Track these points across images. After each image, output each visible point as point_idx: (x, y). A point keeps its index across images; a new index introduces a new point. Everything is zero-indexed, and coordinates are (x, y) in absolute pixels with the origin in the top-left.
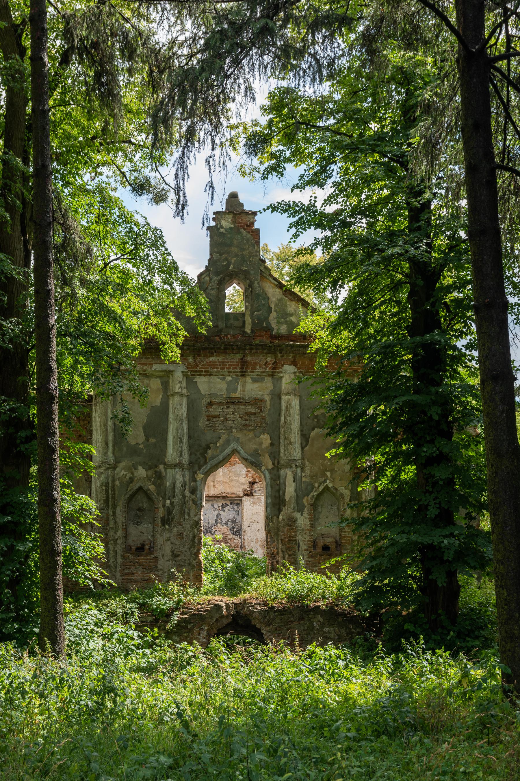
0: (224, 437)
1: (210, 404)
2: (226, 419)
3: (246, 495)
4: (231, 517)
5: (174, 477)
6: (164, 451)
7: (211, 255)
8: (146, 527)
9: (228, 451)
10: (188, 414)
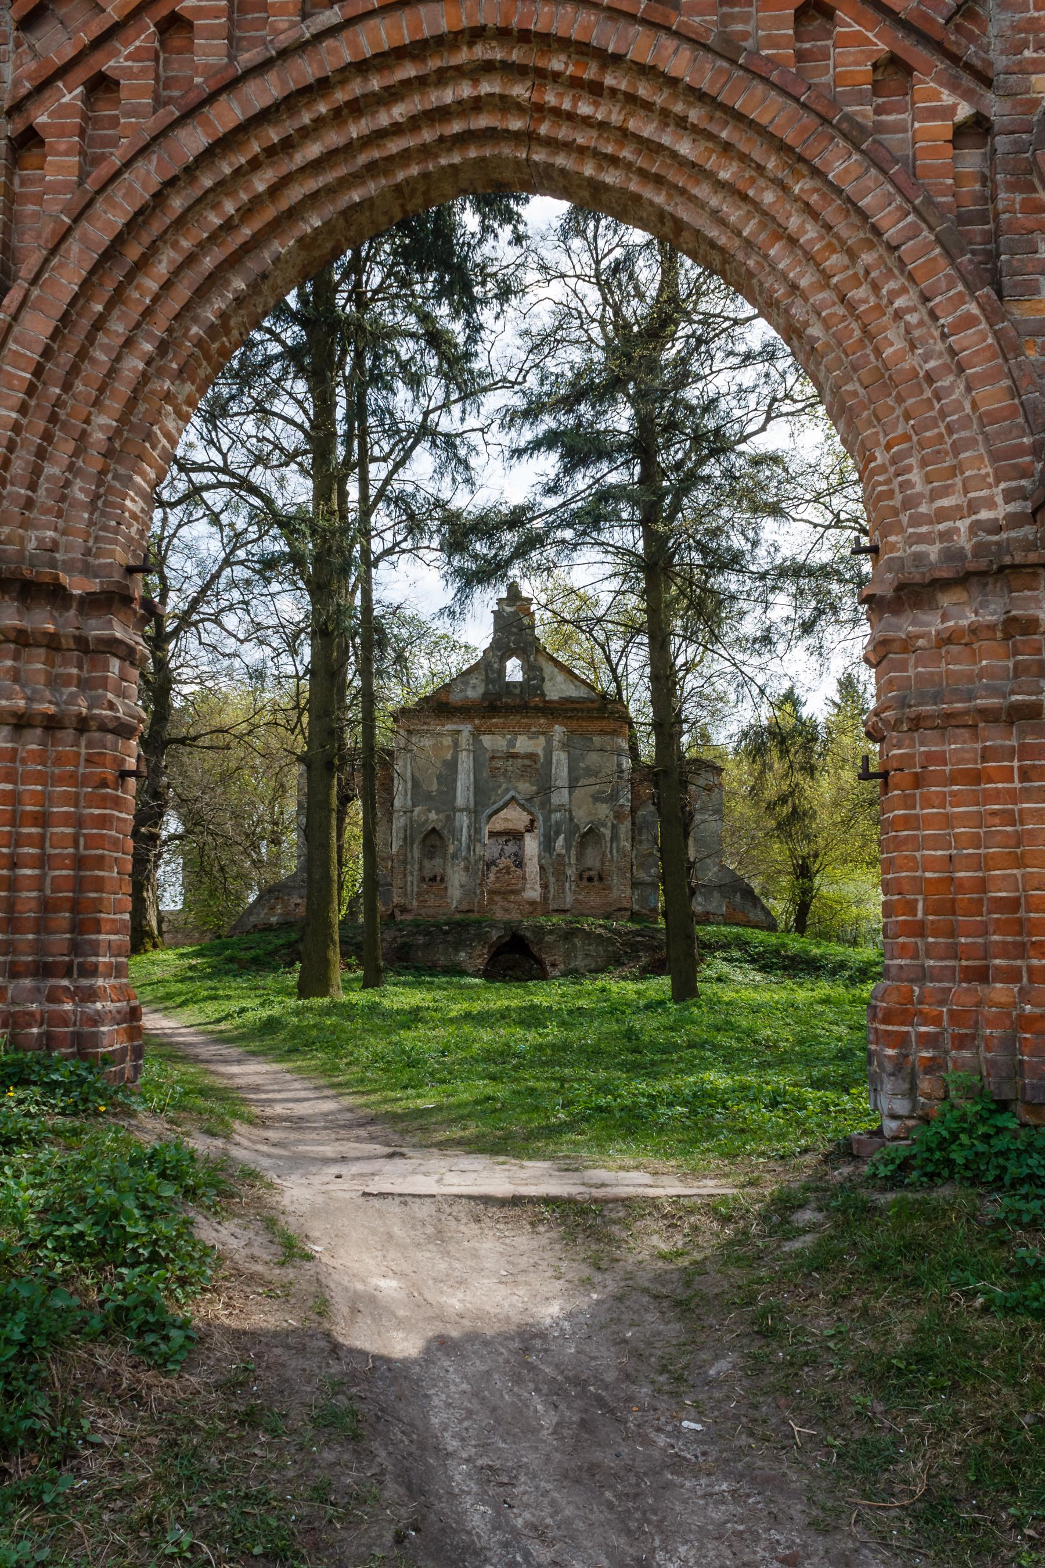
6: (454, 798)
8: (438, 861)
9: (508, 797)
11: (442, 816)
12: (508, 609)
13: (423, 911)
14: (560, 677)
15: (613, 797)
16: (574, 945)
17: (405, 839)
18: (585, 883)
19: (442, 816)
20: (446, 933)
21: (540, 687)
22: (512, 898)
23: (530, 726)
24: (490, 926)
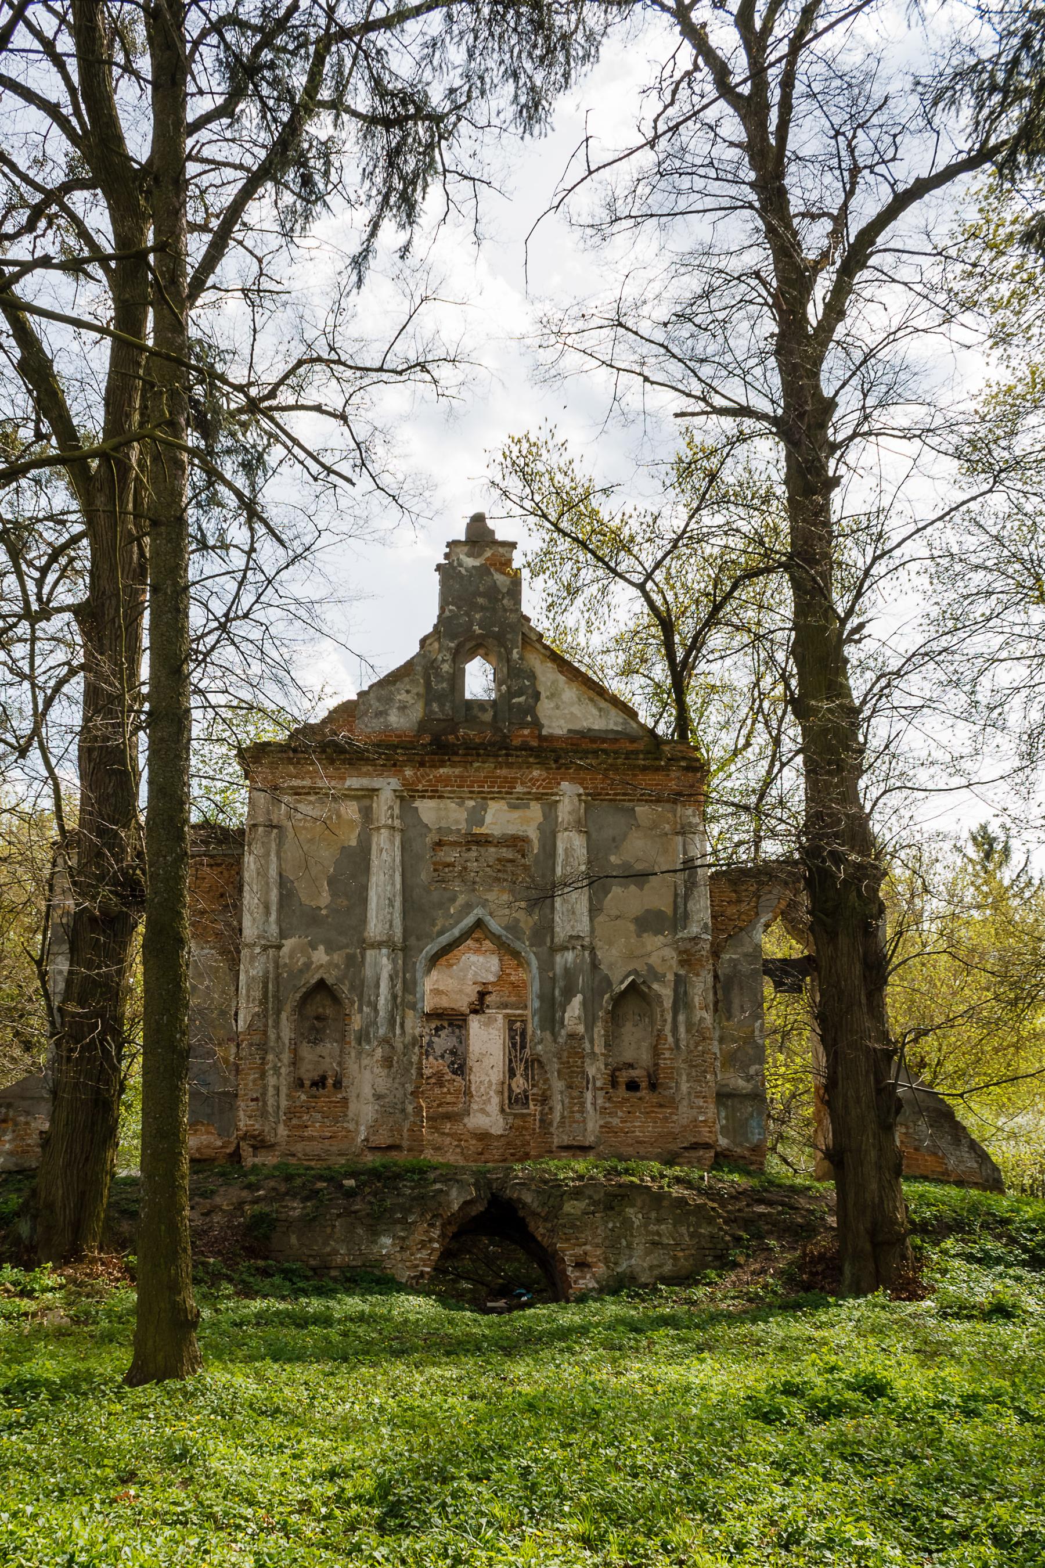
0: (461, 899)
1: (439, 844)
2: (465, 868)
3: (475, 1012)
4: (450, 1045)
5: (376, 964)
6: (364, 921)
7: (442, 609)
8: (329, 1047)
9: (469, 921)
10: (403, 862)
11: (338, 957)
12: (470, 562)
13: (299, 1148)
14: (570, 693)
15: (680, 918)
16: (627, 1223)
17: (264, 1001)
18: (622, 1092)
19: (338, 957)
20: (350, 1194)
21: (532, 710)
22: (447, 1127)
23: (512, 783)
24: (445, 1179)
